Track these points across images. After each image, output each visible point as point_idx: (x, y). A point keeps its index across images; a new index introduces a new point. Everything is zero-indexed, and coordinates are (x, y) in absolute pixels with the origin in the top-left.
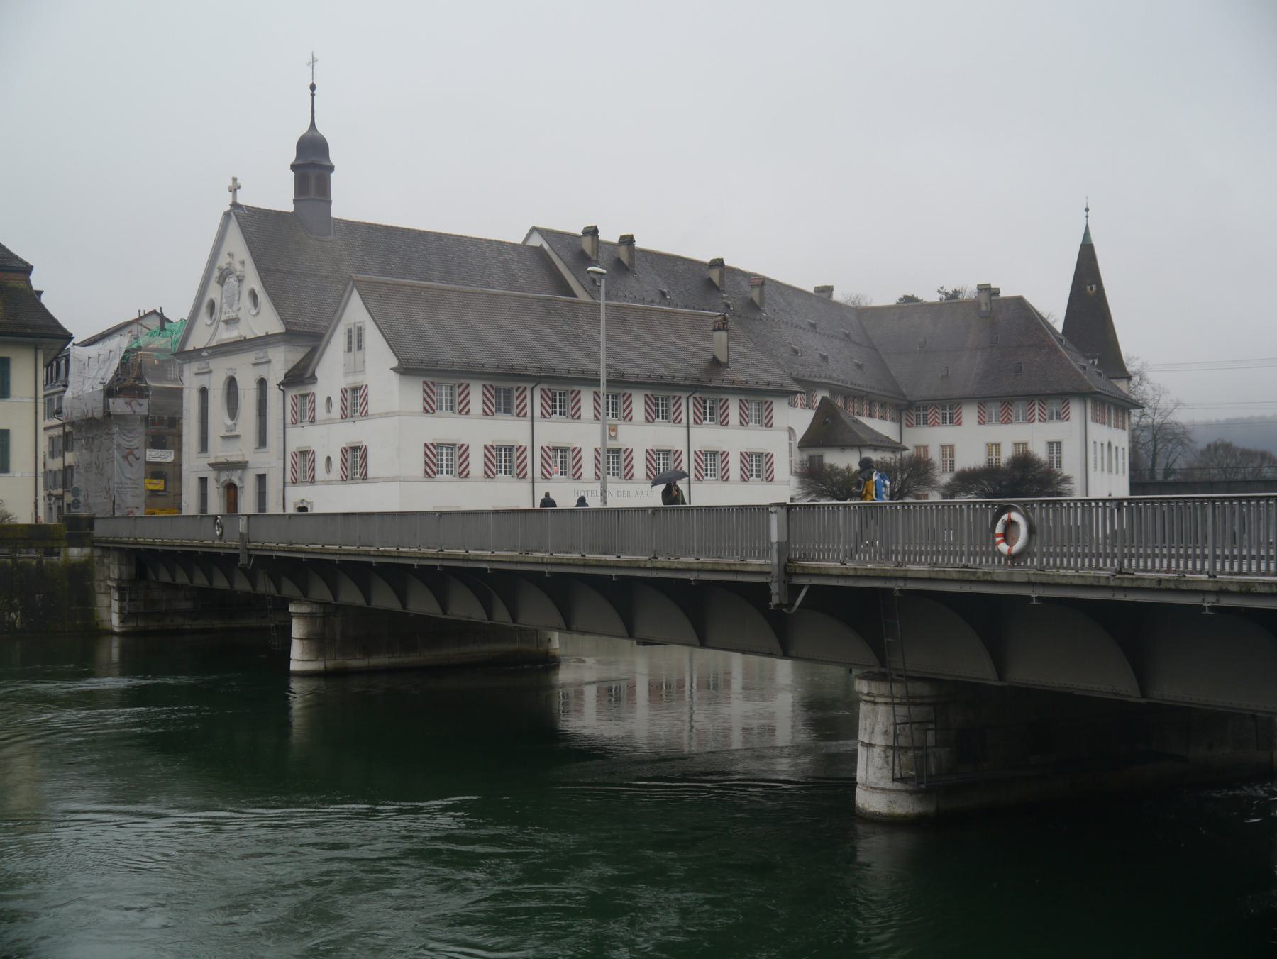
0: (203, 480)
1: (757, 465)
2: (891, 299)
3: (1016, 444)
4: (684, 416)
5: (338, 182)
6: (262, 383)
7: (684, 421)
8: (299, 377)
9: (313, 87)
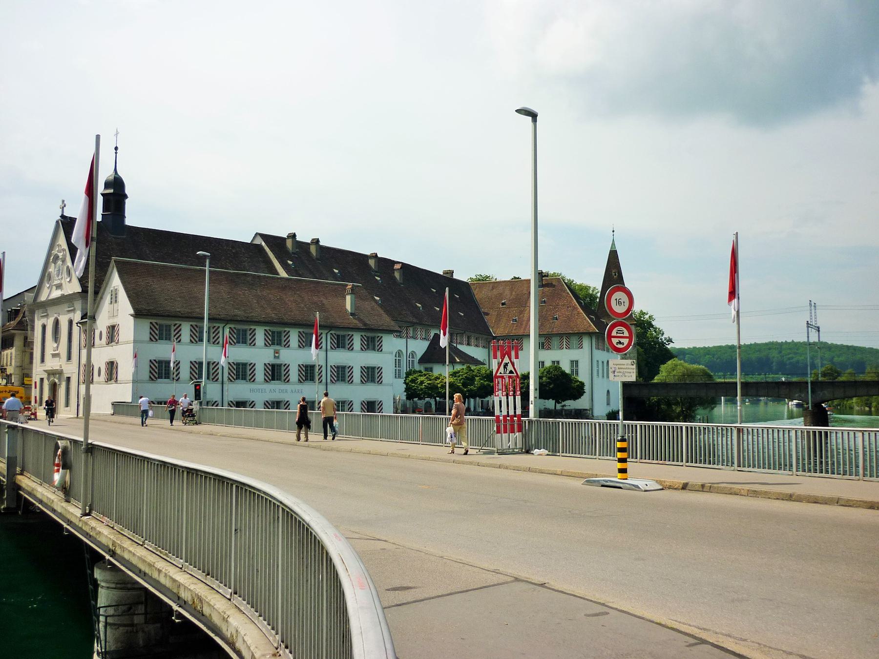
0: (42, 380)
1: (371, 375)
2: (508, 278)
3: (553, 362)
4: (324, 345)
5: (129, 206)
6: (71, 322)
7: (324, 347)
8: (89, 318)
9: (116, 148)
